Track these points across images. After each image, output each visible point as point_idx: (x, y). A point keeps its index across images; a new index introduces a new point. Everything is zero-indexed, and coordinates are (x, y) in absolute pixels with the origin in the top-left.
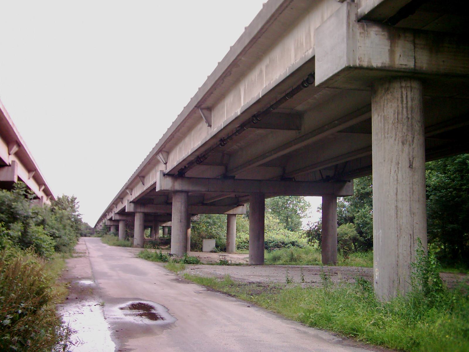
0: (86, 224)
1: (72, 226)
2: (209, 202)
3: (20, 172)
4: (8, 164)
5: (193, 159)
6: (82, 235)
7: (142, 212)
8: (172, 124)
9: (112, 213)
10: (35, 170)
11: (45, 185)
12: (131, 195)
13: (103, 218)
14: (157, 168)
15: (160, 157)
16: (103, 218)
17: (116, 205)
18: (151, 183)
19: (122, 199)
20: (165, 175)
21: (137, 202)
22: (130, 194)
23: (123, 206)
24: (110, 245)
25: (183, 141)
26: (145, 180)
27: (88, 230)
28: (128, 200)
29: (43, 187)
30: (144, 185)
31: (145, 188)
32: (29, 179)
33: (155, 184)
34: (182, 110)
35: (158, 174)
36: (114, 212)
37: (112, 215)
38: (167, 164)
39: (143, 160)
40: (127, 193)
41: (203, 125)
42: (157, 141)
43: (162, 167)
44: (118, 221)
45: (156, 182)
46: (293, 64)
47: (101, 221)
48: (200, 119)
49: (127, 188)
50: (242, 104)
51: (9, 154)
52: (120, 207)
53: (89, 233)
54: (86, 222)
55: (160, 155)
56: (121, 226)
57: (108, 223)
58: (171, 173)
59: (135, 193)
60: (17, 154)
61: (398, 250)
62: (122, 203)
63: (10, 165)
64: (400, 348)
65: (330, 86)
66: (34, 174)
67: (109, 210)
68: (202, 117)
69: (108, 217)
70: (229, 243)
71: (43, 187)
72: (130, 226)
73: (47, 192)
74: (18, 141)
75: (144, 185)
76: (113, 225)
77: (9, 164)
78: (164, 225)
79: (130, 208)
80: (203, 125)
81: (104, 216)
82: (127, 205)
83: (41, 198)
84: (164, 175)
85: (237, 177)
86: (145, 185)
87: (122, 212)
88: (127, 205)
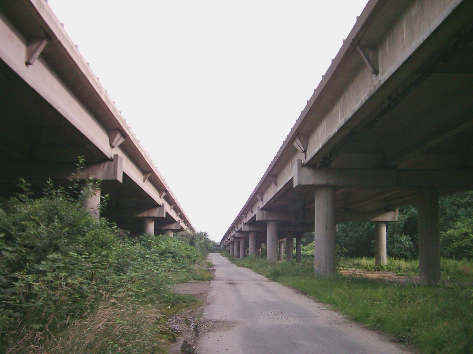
0: (213, 242)
1: (205, 248)
3: (167, 208)
4: (110, 157)
6: (210, 252)
7: (275, 221)
8: (277, 154)
10: (151, 171)
11: (166, 191)
12: (246, 218)
14: (293, 161)
19: (252, 207)
22: (245, 218)
24: (223, 257)
26: (380, 54)
28: (244, 222)
29: (164, 194)
31: (281, 185)
33: (292, 180)
34: (321, 80)
35: (295, 166)
37: (234, 233)
39: (268, 167)
40: (258, 200)
41: (273, 185)
42: (272, 159)
43: (300, 156)
44: (247, 233)
45: (293, 177)
48: (360, 66)
49: (235, 224)
50: (266, 201)
51: (160, 198)
52: (250, 216)
53: (215, 250)
54: (214, 240)
55: (298, 141)
57: (237, 235)
59: (314, 143)
60: (122, 147)
62: (276, 185)
63: (111, 160)
66: (150, 175)
67: (239, 219)
68: (363, 62)
69: (237, 229)
72: (261, 238)
73: (191, 229)
74: (165, 189)
75: (252, 212)
76: (253, 231)
77: (111, 158)
80: (273, 185)
81: (232, 228)
82: (256, 212)
84: (303, 166)
86: (253, 212)
87: (253, 222)
88: (256, 212)
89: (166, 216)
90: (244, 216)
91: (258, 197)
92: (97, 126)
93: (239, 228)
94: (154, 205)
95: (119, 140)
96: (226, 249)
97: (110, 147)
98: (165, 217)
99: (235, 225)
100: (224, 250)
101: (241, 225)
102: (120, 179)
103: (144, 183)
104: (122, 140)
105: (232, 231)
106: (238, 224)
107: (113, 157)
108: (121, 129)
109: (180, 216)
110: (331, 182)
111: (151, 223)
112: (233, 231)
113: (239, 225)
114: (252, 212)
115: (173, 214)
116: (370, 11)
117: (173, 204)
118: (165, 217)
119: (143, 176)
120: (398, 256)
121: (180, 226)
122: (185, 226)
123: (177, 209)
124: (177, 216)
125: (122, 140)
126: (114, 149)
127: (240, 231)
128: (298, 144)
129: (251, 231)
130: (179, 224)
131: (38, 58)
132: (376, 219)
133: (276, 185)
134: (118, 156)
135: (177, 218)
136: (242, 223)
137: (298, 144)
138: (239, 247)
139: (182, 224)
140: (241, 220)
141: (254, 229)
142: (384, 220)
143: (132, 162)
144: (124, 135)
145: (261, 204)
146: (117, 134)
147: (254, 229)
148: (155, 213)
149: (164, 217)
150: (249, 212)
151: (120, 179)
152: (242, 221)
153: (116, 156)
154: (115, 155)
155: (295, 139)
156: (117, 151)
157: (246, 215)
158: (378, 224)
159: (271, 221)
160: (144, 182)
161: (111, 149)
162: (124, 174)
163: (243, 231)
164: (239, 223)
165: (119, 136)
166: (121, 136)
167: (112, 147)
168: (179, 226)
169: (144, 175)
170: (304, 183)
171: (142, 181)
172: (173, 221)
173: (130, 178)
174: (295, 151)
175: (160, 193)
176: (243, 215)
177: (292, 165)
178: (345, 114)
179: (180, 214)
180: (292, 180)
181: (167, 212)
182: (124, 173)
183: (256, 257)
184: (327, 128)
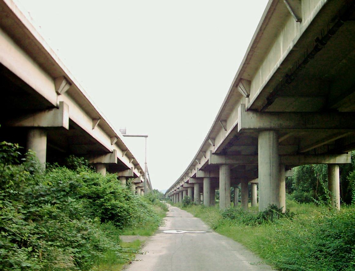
7: (199, 183)
9: (188, 177)
10: (100, 118)
11: (134, 158)
13: (177, 185)
15: (241, 89)
16: (177, 185)
17: (200, 160)
18: (234, 125)
19: (205, 152)
21: (222, 152)
23: (206, 161)
25: (276, 43)
27: (161, 197)
28: (190, 176)
29: (115, 140)
31: (229, 131)
32: (123, 156)
33: (237, 125)
37: (187, 179)
44: (202, 179)
45: (237, 124)
47: (178, 184)
52: (203, 162)
56: (223, 177)
57: (186, 185)
58: (254, 107)
61: (85, 202)
62: (226, 130)
64: (320, 244)
65: (261, 109)
66: (99, 123)
67: (193, 166)
68: (289, 13)
69: (192, 175)
70: (350, 190)
71: (132, 160)
74: (65, 75)
75: (206, 158)
77: (112, 151)
78: (332, 161)
82: (209, 158)
83: (131, 169)
87: (207, 168)
89: (134, 176)
90: (198, 162)
91: (210, 141)
92: (70, 102)
93: (193, 174)
94: (105, 151)
95: (64, 86)
96: (169, 198)
97: (56, 94)
98: (116, 162)
99: (184, 177)
100: (168, 199)
102: (66, 125)
103: (93, 130)
104: (67, 88)
106: (192, 170)
107: (113, 150)
108: (66, 76)
109: (133, 163)
111: (103, 169)
114: (206, 158)
115: (125, 161)
118: (116, 162)
119: (92, 123)
120: (305, 201)
121: (133, 173)
122: (138, 172)
123: (130, 156)
125: (67, 88)
126: (60, 95)
127: (194, 177)
130: (132, 171)
133: (226, 130)
134: (64, 103)
135: (130, 165)
136: (196, 169)
138: (176, 198)
139: (119, 155)
141: (229, 161)
142: (337, 163)
144: (69, 82)
145: (214, 149)
146: (62, 81)
148: (106, 159)
149: (115, 163)
151: (66, 125)
153: (62, 103)
154: (114, 150)
156: (63, 98)
157: (200, 160)
158: (331, 167)
159: (189, 187)
160: (93, 129)
161: (57, 96)
162: (71, 121)
163: (197, 177)
164: (192, 169)
165: (64, 83)
166: (67, 83)
167: (58, 94)
168: (132, 172)
169: (93, 122)
173: (87, 133)
174: (240, 96)
175: (111, 140)
177: (239, 107)
178: (254, 93)
180: (237, 125)
181: (73, 121)
182: (118, 158)
184: (283, 49)
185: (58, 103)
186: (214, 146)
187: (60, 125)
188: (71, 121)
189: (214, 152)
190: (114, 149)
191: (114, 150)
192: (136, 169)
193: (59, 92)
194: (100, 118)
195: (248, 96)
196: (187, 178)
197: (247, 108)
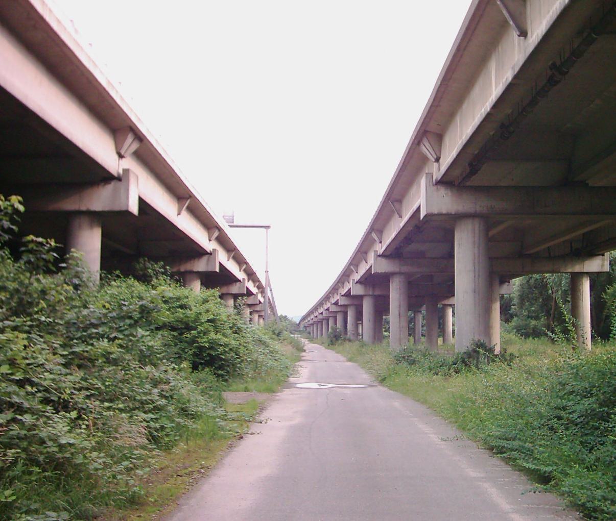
2: (532, 251)
3: (222, 257)
4: (116, 175)
5: (411, 228)
7: (355, 305)
11: (246, 263)
18: (415, 207)
19: (366, 253)
20: (383, 256)
21: (394, 253)
28: (340, 294)
29: (216, 234)
30: (367, 263)
31: (406, 218)
32: (228, 260)
33: (419, 209)
36: (340, 294)
38: (441, 160)
40: (425, 159)
44: (360, 298)
45: (420, 206)
46: (309, 341)
49: (338, 282)
51: (210, 240)
52: (363, 269)
56: (396, 294)
62: (401, 217)
63: (119, 179)
66: (189, 204)
67: (345, 276)
68: (506, 21)
69: (344, 291)
74: (132, 125)
75: (367, 263)
76: (400, 273)
77: (210, 251)
78: (577, 268)
79: (358, 290)
82: (372, 263)
83: (242, 281)
85: (590, 184)
87: (369, 280)
89: (247, 292)
91: (374, 235)
94: (198, 252)
95: (131, 144)
97: (116, 157)
98: (217, 270)
101: (348, 284)
102: (134, 208)
104: (135, 146)
105: (334, 294)
107: (212, 250)
108: (134, 127)
109: (245, 271)
110: (356, 303)
112: (335, 295)
113: (345, 285)
115: (233, 267)
116: (461, 36)
117: (232, 251)
118: (217, 270)
120: (532, 334)
121: (245, 288)
122: (254, 287)
123: (240, 260)
124: (240, 271)
125: (135, 146)
126: (123, 159)
127: (348, 295)
128: (426, 149)
129: (393, 274)
130: (244, 284)
131: (185, 210)
132: (443, 303)
133: (401, 217)
134: (130, 171)
135: (240, 275)
136: (351, 282)
137: (426, 149)
140: (349, 276)
141: (405, 269)
143: (188, 213)
144: (139, 137)
145: (381, 248)
146: (128, 135)
147: (405, 269)
148: (201, 266)
150: (362, 261)
151: (134, 208)
152: (352, 278)
153: (126, 171)
154: (213, 249)
155: (371, 233)
156: (129, 163)
158: (575, 278)
160: (179, 214)
161: (119, 160)
162: (142, 201)
165: (130, 138)
167: (121, 156)
168: (244, 287)
169: (178, 203)
170: (354, 294)
171: (176, 213)
172: (233, 280)
174: (425, 159)
175: (209, 233)
176: (352, 267)
177: (422, 178)
179: (244, 267)
180: (419, 209)
182: (220, 263)
183: (375, 338)
185: (121, 172)
186: (381, 242)
187: (124, 209)
188: (142, 201)
189: (381, 253)
190: (214, 248)
191: (213, 249)
192: (250, 282)
193: (123, 152)
194: (190, 196)
195: (437, 160)
196: (335, 297)
197: (436, 180)
